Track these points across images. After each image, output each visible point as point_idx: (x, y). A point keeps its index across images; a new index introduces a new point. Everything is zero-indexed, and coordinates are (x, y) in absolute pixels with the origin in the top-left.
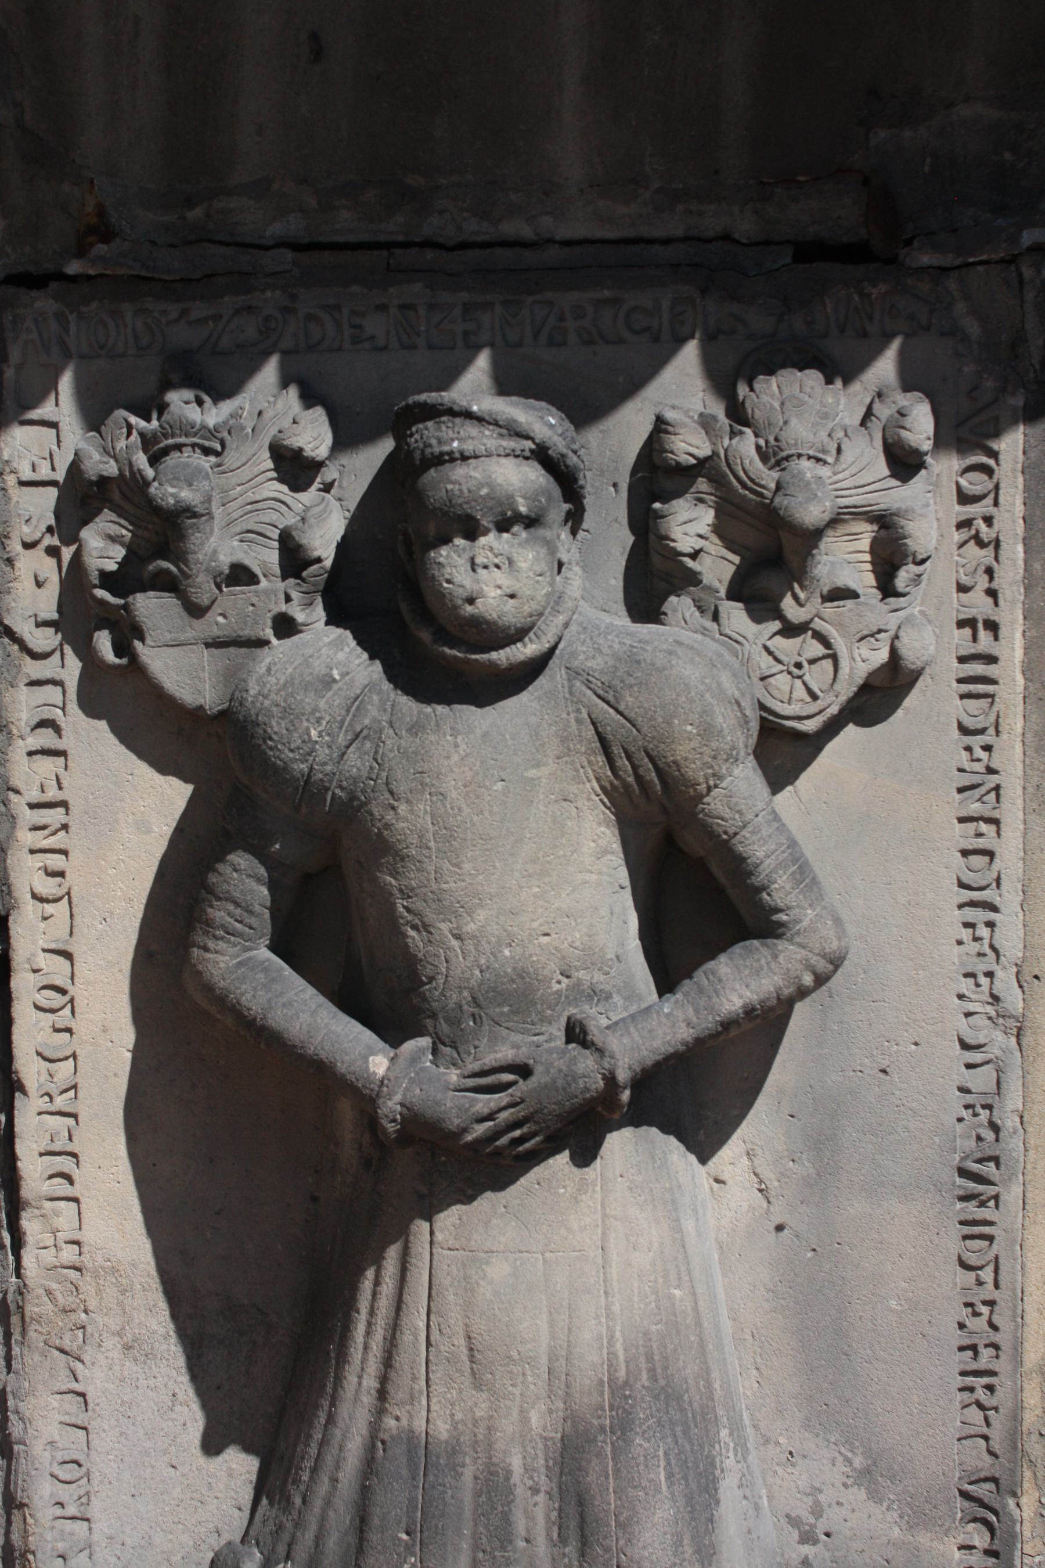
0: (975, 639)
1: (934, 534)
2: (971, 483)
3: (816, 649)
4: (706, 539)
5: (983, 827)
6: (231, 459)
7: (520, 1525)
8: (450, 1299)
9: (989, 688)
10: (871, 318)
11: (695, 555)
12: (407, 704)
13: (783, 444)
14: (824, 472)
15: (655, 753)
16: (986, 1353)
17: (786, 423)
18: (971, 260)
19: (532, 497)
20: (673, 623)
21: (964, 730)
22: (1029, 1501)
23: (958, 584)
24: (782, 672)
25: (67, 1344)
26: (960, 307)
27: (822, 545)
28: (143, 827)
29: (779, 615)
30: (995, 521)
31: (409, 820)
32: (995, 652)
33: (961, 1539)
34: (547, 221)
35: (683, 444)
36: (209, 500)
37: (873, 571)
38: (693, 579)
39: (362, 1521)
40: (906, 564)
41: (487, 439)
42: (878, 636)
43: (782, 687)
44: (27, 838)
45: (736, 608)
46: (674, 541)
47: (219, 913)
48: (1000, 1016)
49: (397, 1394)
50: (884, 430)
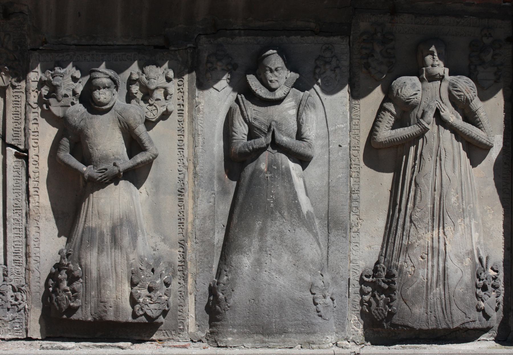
3: (155, 108)
6: (65, 78)
7: (105, 240)
8: (95, 205)
11: (136, 93)
12: (90, 115)
16: (182, 220)
19: (108, 84)
21: (179, 121)
22: (189, 244)
25: (36, 219)
26: (178, 56)
28: (50, 135)
29: (149, 103)
31: (90, 132)
33: (179, 250)
34: (115, 42)
36: (61, 84)
38: (135, 97)
39: (82, 240)
41: (102, 75)
44: (32, 137)
47: (62, 147)
48: (184, 166)
49: (87, 221)
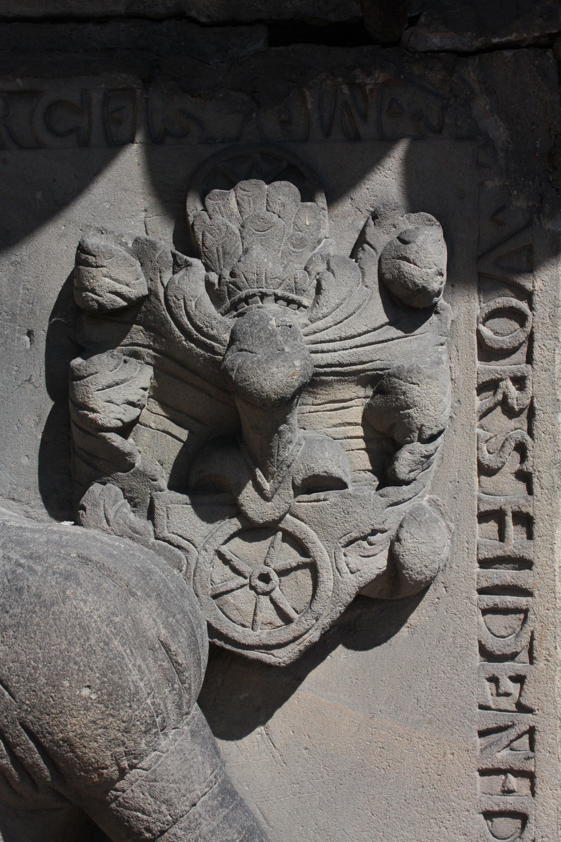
0: (502, 537)
1: (448, 401)
2: (496, 333)
3: (289, 556)
4: (142, 407)
5: (513, 782)
9: (522, 601)
10: (365, 117)
11: (125, 430)
13: (241, 280)
14: (298, 318)
15: (35, 728)
17: (246, 251)
18: (495, 40)
20: (92, 523)
21: (487, 654)
23: (480, 464)
24: (242, 586)
27: (294, 418)
29: (237, 511)
30: (529, 383)
32: (529, 554)
35: (107, 280)
37: (366, 450)
38: (121, 462)
40: (412, 442)
42: (371, 538)
43: (243, 607)
45: (179, 502)
46: (94, 411)
50: (380, 261)
